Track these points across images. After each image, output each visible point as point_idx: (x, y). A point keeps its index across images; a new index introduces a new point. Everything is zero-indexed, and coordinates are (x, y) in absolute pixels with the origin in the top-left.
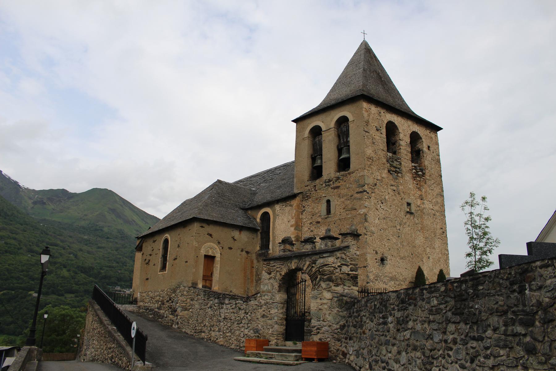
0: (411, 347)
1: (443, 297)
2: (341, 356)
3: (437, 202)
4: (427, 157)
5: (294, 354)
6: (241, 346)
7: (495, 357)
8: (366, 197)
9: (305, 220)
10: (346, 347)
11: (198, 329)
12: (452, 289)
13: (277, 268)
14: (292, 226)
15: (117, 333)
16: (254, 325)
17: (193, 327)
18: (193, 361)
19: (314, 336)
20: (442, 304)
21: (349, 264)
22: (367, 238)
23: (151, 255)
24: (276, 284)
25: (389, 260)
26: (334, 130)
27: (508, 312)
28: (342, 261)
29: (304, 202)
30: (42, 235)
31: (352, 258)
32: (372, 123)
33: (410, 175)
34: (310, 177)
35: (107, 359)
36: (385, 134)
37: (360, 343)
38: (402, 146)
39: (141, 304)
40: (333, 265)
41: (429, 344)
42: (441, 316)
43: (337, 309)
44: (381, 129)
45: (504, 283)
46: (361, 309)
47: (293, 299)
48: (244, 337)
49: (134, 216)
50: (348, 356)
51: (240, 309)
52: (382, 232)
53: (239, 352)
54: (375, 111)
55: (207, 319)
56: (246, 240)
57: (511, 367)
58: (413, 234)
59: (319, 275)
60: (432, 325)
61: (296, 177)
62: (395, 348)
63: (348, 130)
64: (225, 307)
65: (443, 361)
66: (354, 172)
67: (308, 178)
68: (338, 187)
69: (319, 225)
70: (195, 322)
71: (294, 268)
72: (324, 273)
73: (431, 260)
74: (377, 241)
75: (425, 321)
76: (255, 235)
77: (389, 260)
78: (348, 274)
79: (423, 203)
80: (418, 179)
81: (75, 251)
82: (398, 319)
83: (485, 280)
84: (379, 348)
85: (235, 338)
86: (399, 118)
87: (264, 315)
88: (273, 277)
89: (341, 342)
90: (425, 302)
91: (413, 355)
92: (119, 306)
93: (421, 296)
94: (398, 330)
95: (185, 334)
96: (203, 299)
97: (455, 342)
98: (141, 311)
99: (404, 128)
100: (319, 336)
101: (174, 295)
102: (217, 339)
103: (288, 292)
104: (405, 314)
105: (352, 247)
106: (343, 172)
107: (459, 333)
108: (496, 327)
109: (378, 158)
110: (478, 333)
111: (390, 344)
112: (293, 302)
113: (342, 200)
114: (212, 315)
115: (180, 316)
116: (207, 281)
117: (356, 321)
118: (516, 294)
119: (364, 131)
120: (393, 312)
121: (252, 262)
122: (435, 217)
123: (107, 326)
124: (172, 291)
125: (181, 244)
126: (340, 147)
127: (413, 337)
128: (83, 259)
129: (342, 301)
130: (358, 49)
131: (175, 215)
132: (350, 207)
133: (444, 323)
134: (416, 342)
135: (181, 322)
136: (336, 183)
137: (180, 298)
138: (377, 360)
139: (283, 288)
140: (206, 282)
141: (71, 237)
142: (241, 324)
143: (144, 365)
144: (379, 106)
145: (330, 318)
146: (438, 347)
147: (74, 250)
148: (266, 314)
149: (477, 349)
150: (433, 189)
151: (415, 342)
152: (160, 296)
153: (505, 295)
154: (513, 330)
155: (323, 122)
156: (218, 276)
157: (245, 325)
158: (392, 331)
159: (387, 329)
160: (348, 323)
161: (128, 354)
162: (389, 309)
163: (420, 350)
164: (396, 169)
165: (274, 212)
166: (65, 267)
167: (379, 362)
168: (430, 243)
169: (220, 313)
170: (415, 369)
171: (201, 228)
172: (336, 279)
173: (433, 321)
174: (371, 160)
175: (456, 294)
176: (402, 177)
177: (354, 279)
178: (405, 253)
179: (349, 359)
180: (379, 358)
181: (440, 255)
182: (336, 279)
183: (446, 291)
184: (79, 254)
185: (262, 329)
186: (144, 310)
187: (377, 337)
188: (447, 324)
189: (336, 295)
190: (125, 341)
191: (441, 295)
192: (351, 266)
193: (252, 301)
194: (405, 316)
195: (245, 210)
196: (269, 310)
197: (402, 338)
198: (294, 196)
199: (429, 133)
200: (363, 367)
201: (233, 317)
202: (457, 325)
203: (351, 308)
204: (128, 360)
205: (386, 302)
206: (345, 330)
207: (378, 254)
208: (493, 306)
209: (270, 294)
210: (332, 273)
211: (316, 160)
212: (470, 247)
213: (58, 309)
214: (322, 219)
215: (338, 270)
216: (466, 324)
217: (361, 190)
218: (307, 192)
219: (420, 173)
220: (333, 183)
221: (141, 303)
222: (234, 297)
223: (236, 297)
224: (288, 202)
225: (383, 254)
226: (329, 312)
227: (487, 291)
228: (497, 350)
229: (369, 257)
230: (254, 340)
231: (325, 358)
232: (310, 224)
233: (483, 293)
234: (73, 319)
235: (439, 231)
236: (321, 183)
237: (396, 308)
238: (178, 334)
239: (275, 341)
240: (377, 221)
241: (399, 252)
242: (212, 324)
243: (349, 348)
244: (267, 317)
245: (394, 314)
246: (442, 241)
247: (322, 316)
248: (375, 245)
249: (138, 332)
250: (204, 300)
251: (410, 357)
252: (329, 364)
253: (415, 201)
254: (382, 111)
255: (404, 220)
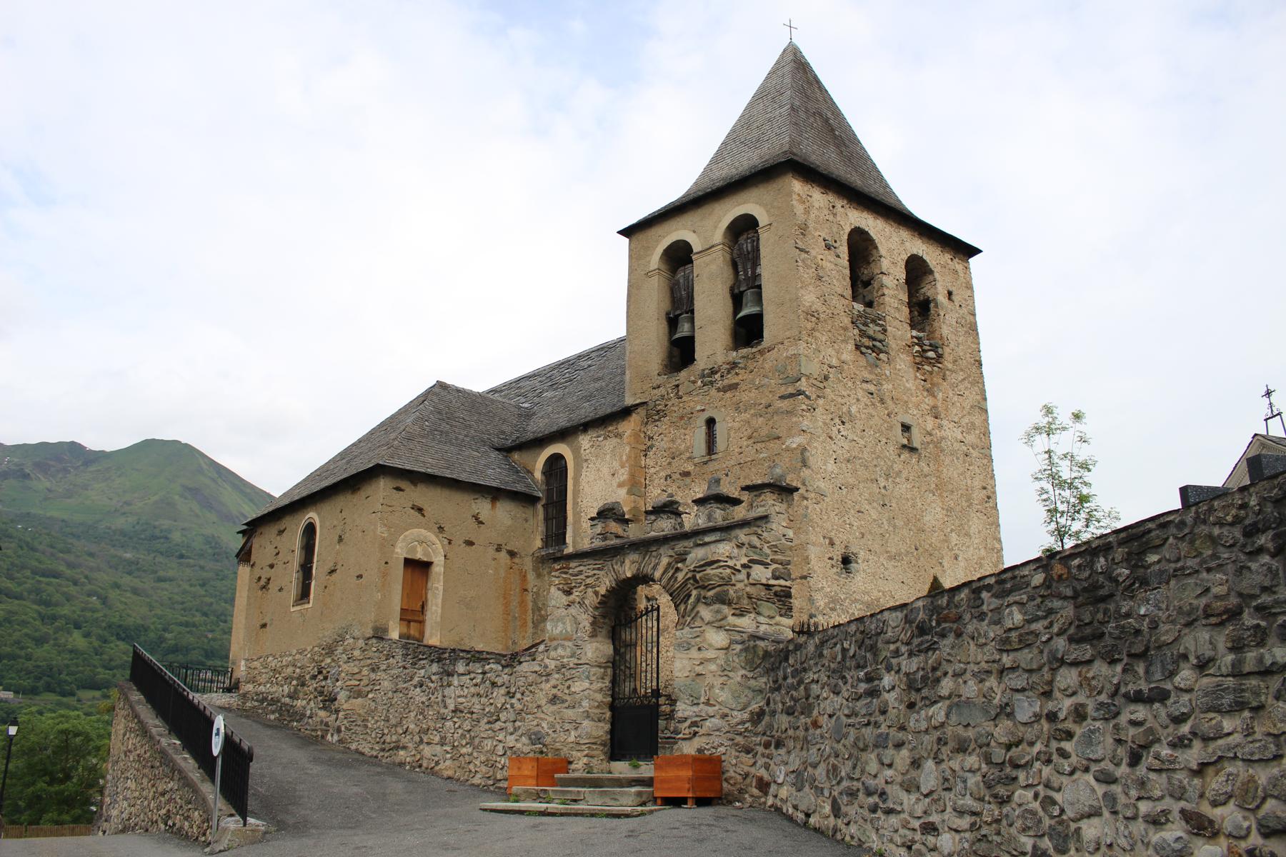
0: (951, 745)
1: (1039, 600)
2: (755, 791)
3: (973, 424)
4: (947, 316)
5: (633, 790)
6: (499, 777)
7: (1206, 740)
8: (804, 407)
9: (652, 470)
10: (767, 767)
11: (388, 740)
12: (1065, 576)
13: (588, 577)
14: (620, 485)
15: (182, 754)
16: (530, 723)
17: (377, 737)
18: (374, 816)
19: (684, 743)
20: (1036, 619)
21: (769, 561)
22: (807, 508)
23: (272, 566)
24: (585, 616)
25: (863, 562)
26: (723, 249)
27: (1241, 613)
28: (752, 554)
29: (649, 427)
30: (20, 552)
31: (775, 546)
32: (816, 229)
33: (909, 359)
34: (666, 366)
35: (156, 822)
36: (847, 258)
37: (804, 753)
38: (888, 288)
39: (250, 687)
40: (730, 563)
41: (1002, 731)
42: (1036, 651)
43: (743, 672)
44: (835, 245)
45: (1226, 533)
46: (805, 665)
47: (628, 657)
48: (504, 754)
49: (244, 506)
50: (773, 788)
51: (494, 684)
52: (845, 491)
53: (492, 792)
54: (822, 201)
55: (413, 714)
56: (508, 522)
57: (1260, 760)
58: (918, 500)
59: (695, 588)
60: (1010, 678)
61: (630, 366)
62: (904, 752)
63: (756, 250)
64: (456, 683)
65: (1047, 771)
66: (773, 349)
67: (661, 367)
68: (734, 387)
69: (688, 480)
70: (383, 723)
71: (629, 575)
72: (706, 584)
73: (962, 564)
74: (832, 514)
75: (988, 672)
76: (529, 512)
77: (863, 562)
78: (768, 587)
79: (940, 427)
80: (926, 367)
81: (102, 589)
82: (912, 677)
83: (1165, 536)
84: (858, 759)
85: (483, 758)
86: (878, 221)
87: (555, 696)
88: (578, 600)
89: (754, 756)
90: (986, 621)
91: (955, 764)
92: (196, 697)
93: (973, 607)
94: (911, 706)
95: (357, 756)
96: (400, 665)
97: (1079, 714)
98: (249, 704)
99: (890, 245)
100: (698, 742)
101: (329, 660)
102: (437, 763)
103: (614, 636)
104: (930, 662)
105: (774, 518)
106: (746, 350)
107: (1092, 689)
108: (1206, 656)
109: (831, 315)
110: (1150, 683)
111: (890, 745)
112: (628, 665)
113: (746, 416)
114: (423, 703)
115: (344, 710)
116: (412, 623)
117: (792, 698)
118: (1266, 559)
119: (797, 248)
120: (894, 661)
121: (524, 577)
122: (968, 459)
123: (158, 738)
124: (323, 652)
125: (347, 535)
126: (736, 291)
127: (954, 718)
128: (122, 607)
129: (755, 652)
130: (778, 62)
131: (332, 467)
132: (764, 432)
133: (1046, 669)
134: (963, 729)
135: (346, 728)
136: (729, 376)
137: (345, 666)
138: (855, 788)
139: (602, 628)
140: (409, 627)
141: (91, 555)
142: (498, 723)
143: (245, 825)
144: (830, 190)
145: (723, 696)
146: (1029, 734)
147: (100, 587)
148: (559, 694)
149: (1148, 725)
150: (961, 393)
151: (960, 730)
152: (294, 665)
153: (1229, 566)
154: (1260, 660)
155: (694, 232)
156: (440, 611)
157: (507, 724)
158: (895, 711)
159: (880, 707)
160: (772, 704)
161: (204, 800)
162: (884, 654)
163: (978, 750)
164: (874, 343)
165: (576, 452)
166: (78, 626)
167: (861, 795)
168: (957, 523)
169: (444, 697)
170: (962, 802)
171: (395, 491)
172: (739, 598)
173: (1013, 669)
174: (814, 319)
175: (1079, 588)
176: (889, 362)
177: (783, 598)
178: (901, 546)
179: (776, 796)
180: (860, 784)
181: (983, 552)
182: (739, 598)
183: (1047, 584)
184: (113, 595)
185: (550, 732)
186: (256, 704)
187: (852, 731)
188: (1054, 670)
189: (738, 638)
190: (201, 771)
191: (1033, 596)
192: (775, 566)
193: (524, 664)
194: (929, 666)
195: (506, 450)
196: (567, 684)
197: (924, 726)
198: (626, 412)
199: (949, 261)
200: (814, 812)
201: (478, 707)
202: (1084, 670)
203: (778, 668)
204: (205, 816)
205: (874, 638)
206: (763, 723)
207: (836, 547)
208: (1195, 602)
209: (570, 644)
210: (727, 582)
211: (679, 325)
212: (1052, 533)
213: (53, 718)
214: (695, 465)
215: (742, 576)
216: (1113, 662)
217: (791, 390)
218: (657, 402)
219: (931, 354)
220: (722, 376)
221: (248, 685)
222: (477, 657)
223: (485, 656)
224: (610, 428)
225: (846, 546)
226: (721, 680)
227: (1173, 565)
228: (1211, 719)
229: (813, 552)
230: (531, 759)
231: (712, 796)
232: (666, 480)
233: (1161, 572)
234: (91, 743)
235: (978, 495)
236: (692, 378)
237: (904, 649)
238: (339, 756)
239: (585, 760)
240: (831, 466)
241: (887, 542)
242: (424, 726)
243: (776, 768)
244: (564, 701)
245: (899, 664)
246: (985, 517)
247: (703, 692)
248: (828, 525)
249: (228, 740)
250: (405, 668)
251: (948, 773)
252: (726, 811)
253: (920, 422)
254: (839, 203)
255: (895, 466)
